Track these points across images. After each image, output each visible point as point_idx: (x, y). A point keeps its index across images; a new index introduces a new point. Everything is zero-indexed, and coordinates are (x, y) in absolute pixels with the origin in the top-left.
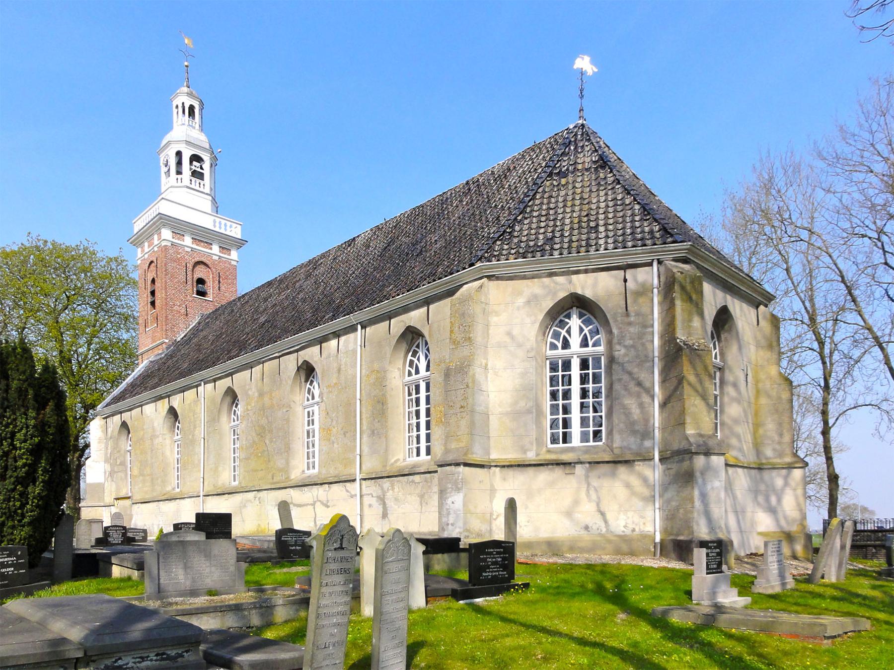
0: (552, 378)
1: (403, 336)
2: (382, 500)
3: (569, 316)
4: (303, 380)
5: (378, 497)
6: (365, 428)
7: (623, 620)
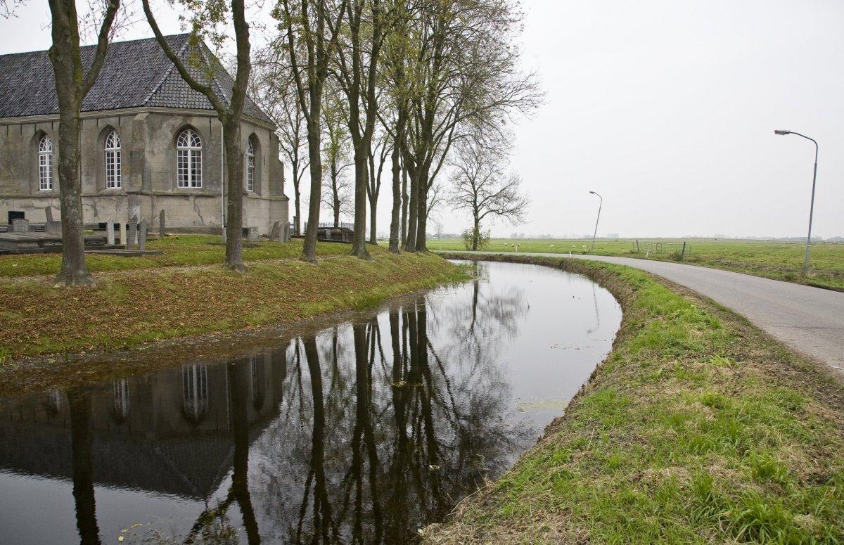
0: (179, 164)
1: (104, 130)
2: (94, 207)
3: (186, 132)
4: (38, 140)
5: (92, 206)
6: (83, 170)
7: (327, 89)
